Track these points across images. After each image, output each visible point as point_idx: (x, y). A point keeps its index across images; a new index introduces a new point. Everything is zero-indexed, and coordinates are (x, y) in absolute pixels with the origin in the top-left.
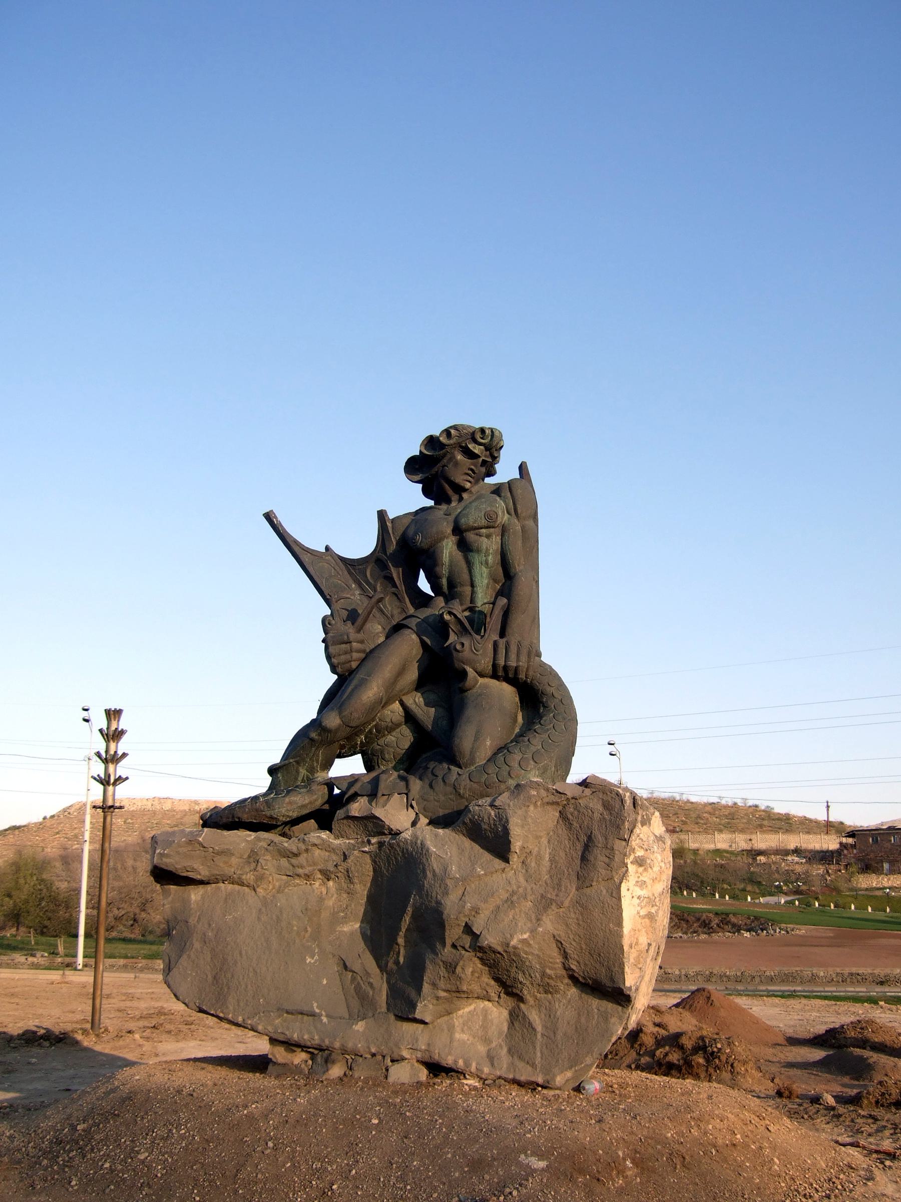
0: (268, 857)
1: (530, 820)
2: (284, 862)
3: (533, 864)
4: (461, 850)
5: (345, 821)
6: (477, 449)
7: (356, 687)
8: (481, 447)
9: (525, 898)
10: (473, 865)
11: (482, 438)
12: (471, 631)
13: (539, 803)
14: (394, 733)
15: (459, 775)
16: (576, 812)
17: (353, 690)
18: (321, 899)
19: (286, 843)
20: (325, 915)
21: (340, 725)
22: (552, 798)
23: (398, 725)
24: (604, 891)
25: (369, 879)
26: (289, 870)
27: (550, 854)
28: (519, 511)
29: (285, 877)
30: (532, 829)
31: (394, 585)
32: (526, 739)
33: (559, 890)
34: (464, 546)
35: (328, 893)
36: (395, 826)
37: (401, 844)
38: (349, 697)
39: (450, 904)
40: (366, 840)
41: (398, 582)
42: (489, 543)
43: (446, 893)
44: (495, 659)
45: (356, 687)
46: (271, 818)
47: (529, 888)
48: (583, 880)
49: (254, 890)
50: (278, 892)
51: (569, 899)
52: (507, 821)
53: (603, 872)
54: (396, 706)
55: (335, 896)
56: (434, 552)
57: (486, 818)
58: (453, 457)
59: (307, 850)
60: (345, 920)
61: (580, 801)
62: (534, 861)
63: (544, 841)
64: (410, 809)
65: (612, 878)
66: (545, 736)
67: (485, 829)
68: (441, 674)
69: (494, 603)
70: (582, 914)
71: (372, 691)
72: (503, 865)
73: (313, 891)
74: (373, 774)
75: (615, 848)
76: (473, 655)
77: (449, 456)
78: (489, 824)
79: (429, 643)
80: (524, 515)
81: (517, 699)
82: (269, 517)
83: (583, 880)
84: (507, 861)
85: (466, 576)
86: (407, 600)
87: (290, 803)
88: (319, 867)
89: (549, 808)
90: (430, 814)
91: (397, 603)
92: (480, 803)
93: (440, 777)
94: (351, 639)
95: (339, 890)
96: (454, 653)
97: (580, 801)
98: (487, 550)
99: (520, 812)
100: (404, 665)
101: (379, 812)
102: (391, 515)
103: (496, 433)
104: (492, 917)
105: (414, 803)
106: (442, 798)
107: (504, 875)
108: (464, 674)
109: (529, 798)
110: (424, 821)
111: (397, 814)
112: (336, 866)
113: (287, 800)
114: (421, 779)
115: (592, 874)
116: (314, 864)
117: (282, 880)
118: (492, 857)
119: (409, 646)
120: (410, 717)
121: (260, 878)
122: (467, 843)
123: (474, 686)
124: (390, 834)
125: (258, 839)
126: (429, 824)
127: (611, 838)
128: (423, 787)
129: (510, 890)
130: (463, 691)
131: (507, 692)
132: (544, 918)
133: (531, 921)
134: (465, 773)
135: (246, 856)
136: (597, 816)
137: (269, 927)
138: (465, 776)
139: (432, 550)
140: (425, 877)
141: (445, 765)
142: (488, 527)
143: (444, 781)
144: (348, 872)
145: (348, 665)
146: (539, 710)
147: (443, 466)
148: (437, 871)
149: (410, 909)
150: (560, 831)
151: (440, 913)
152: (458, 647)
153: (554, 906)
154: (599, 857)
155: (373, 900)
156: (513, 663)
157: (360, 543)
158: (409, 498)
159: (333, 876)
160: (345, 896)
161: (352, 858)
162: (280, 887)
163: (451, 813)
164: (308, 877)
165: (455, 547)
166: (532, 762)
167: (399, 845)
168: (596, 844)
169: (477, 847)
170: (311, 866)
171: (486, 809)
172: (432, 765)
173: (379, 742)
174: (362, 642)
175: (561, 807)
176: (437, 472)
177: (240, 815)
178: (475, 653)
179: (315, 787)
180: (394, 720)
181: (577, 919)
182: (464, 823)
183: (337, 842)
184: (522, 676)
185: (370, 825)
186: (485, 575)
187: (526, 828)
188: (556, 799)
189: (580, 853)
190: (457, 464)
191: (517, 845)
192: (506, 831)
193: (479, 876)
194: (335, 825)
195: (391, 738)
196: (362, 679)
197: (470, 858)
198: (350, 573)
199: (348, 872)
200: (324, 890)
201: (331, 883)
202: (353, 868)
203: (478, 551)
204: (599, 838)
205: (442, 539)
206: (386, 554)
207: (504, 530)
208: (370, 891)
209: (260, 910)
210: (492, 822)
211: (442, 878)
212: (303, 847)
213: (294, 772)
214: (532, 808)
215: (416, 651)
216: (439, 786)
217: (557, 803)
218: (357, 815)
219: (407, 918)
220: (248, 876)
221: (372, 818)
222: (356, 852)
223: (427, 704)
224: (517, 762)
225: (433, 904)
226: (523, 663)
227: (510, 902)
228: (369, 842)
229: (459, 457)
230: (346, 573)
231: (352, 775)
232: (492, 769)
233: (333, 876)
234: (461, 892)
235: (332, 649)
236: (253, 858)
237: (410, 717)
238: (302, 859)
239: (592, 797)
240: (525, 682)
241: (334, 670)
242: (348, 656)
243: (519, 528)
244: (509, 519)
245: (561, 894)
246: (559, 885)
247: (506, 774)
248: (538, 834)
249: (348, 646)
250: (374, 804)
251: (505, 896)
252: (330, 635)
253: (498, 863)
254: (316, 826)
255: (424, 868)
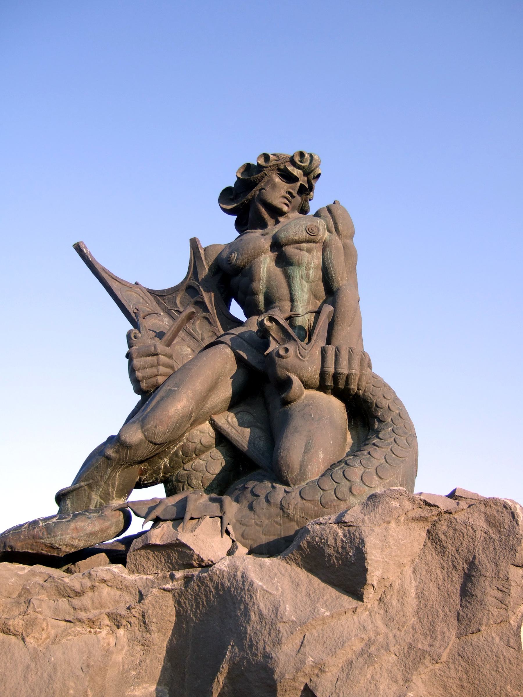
0: (44, 597)
1: (391, 541)
2: (63, 603)
3: (394, 602)
4: (296, 585)
5: (143, 552)
6: (297, 172)
7: (162, 399)
8: (300, 174)
9: (387, 649)
10: (313, 603)
11: (301, 162)
12: (297, 339)
13: (402, 519)
14: (203, 457)
15: (286, 492)
16: (451, 531)
17: (158, 402)
18: (108, 653)
19: (67, 579)
20: (112, 673)
21: (141, 440)
22: (418, 512)
23: (207, 448)
24: (497, 639)
25: (171, 626)
26: (69, 614)
27: (417, 588)
28: (341, 229)
29: (64, 623)
30: (393, 553)
31: (206, 310)
32: (366, 453)
33: (434, 638)
34: (283, 261)
35: (116, 645)
36: (206, 555)
37: (215, 578)
38: (153, 410)
39: (284, 658)
40: (168, 574)
41: (209, 307)
42: (310, 257)
43: (278, 642)
44: (323, 366)
45: (162, 399)
46: (52, 547)
47: (391, 636)
48: (466, 624)
49: (23, 640)
50: (53, 643)
51: (448, 650)
52: (362, 542)
53: (495, 611)
54: (206, 426)
55: (126, 648)
56: (251, 267)
57: (331, 539)
58: (270, 180)
59: (93, 588)
60: (137, 680)
61: (456, 516)
62: (395, 597)
63: (408, 571)
64: (225, 535)
65: (506, 621)
66: (387, 450)
67: (330, 555)
68: (260, 388)
69: (318, 313)
70: (466, 672)
71: (179, 405)
72: (354, 603)
73: (99, 641)
74: (177, 498)
75: (511, 577)
76: (298, 361)
77: (266, 179)
78: (336, 548)
79: (245, 356)
80: (345, 232)
81: (346, 416)
82: (78, 248)
83: (466, 624)
84: (359, 597)
85: (284, 291)
86: (219, 324)
87: (76, 529)
88: (107, 610)
89: (415, 525)
90: (250, 542)
91: (208, 327)
92: (321, 520)
93: (262, 498)
94: (159, 350)
95: (132, 640)
96: (277, 360)
97: (456, 516)
98: (308, 263)
99: (378, 530)
100: (218, 379)
101: (186, 538)
102: (204, 244)
103: (316, 157)
104: (343, 676)
105: (230, 528)
106: (266, 522)
107: (355, 617)
108: (287, 383)
109: (390, 511)
110: (242, 550)
111: (208, 541)
112: (129, 608)
113: (73, 525)
114: (237, 501)
115: (479, 615)
116: (102, 606)
117: (59, 626)
118: (338, 593)
119: (222, 364)
120: (222, 439)
121: (31, 624)
122: (303, 575)
123: (299, 397)
124: (200, 566)
125: (33, 574)
126: (249, 553)
127: (504, 563)
128: (240, 510)
129: (366, 638)
130: (286, 402)
131: (336, 407)
132: (414, 677)
133: (396, 682)
134: (294, 491)
135: (15, 596)
136: (480, 534)
137: (37, 690)
138: (295, 494)
139: (248, 267)
140: (248, 620)
141: (268, 484)
142: (308, 241)
143: (267, 501)
144: (143, 616)
145: (154, 380)
146: (373, 425)
147: (260, 190)
148: (265, 611)
149: (225, 667)
150: (429, 557)
151: (270, 672)
152: (282, 352)
153: (427, 661)
154: (487, 590)
155: (174, 655)
156: (344, 370)
157: (171, 272)
158: (220, 231)
159: (124, 622)
160: (139, 648)
161: (150, 598)
162: (56, 636)
163: (278, 539)
164: (92, 623)
165: (273, 263)
166: (376, 477)
167: (211, 580)
168: (483, 572)
169: (316, 581)
170: (97, 608)
171: (331, 528)
172: (251, 485)
173: (186, 467)
174: (170, 357)
175: (429, 525)
176: (253, 197)
177: (13, 543)
178: (301, 362)
179: (108, 512)
180: (204, 441)
181: (460, 679)
182: (300, 548)
183: (132, 577)
184: (354, 386)
185: (175, 556)
186: (306, 290)
187: (387, 551)
188: (425, 512)
189: (458, 587)
190: (274, 186)
191: (374, 575)
192: (361, 556)
193: (323, 619)
194: (130, 558)
195: (199, 462)
196: (170, 390)
197: (308, 594)
198: (159, 303)
199: (143, 616)
200: (112, 641)
201: (121, 632)
202: (150, 612)
203: (299, 264)
204: (486, 565)
205: (258, 255)
206: (197, 280)
207: (325, 247)
208: (171, 641)
209: (28, 667)
210: (339, 544)
211: (272, 622)
212: (89, 584)
213: (85, 499)
214: (393, 525)
215: (232, 367)
216: (262, 505)
217: (425, 519)
218: (158, 542)
219: (221, 679)
220: (16, 622)
221: (178, 546)
222: (155, 591)
223: (241, 424)
224: (359, 477)
225: (260, 658)
226: (356, 370)
227: (366, 654)
228: (172, 577)
229: (277, 180)
230: (155, 303)
231: (153, 500)
232: (328, 484)
233: (124, 622)
234: (298, 641)
235: (136, 362)
236: (25, 597)
237: (222, 439)
238: (86, 600)
239: (469, 510)
240: (357, 394)
241: (138, 390)
242: (154, 370)
243: (340, 244)
244: (330, 236)
245: (437, 644)
246: (432, 630)
247: (346, 490)
248: (401, 561)
249: (154, 358)
250: (180, 529)
251: (358, 646)
252: (134, 348)
253: (347, 601)
254: (108, 560)
255: (246, 608)
